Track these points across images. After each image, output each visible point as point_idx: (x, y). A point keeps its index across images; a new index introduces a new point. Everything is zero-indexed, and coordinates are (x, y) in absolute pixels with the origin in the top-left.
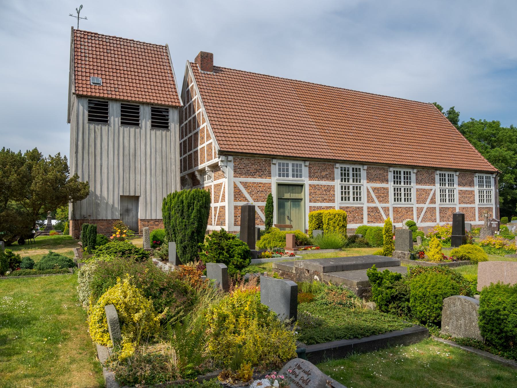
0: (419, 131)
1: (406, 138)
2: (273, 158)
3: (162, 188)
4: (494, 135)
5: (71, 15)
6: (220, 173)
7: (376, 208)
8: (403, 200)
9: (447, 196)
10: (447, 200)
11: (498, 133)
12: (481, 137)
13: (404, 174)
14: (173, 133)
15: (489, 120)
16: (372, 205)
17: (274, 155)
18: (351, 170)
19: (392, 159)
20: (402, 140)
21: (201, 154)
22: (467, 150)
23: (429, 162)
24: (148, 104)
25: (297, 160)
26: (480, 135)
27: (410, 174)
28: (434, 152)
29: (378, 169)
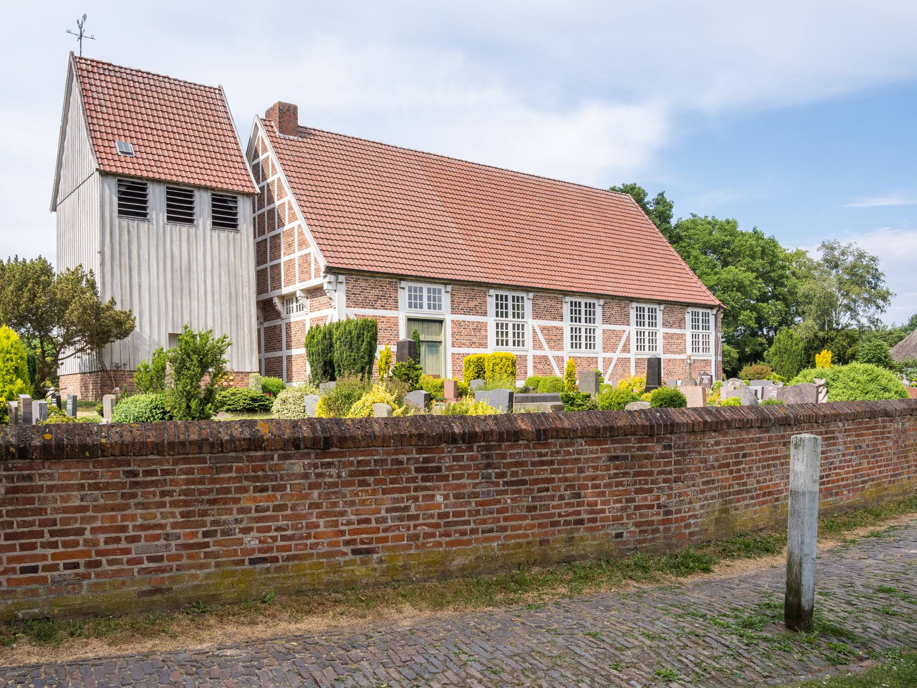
0: (607, 239)
1: (589, 250)
2: (401, 280)
3: (231, 323)
4: (726, 244)
5: (69, 32)
6: (322, 299)
7: (545, 358)
8: (583, 345)
9: (646, 341)
10: (647, 348)
11: (734, 241)
12: (707, 248)
13: (513, 301)
14: (244, 237)
15: (721, 218)
16: (540, 353)
17: (402, 275)
18: (510, 299)
19: (568, 284)
20: (583, 254)
21: (287, 271)
22: (678, 270)
23: (622, 290)
24: (206, 188)
25: (435, 283)
26: (705, 243)
27: (523, 301)
28: (630, 273)
29: (549, 297)
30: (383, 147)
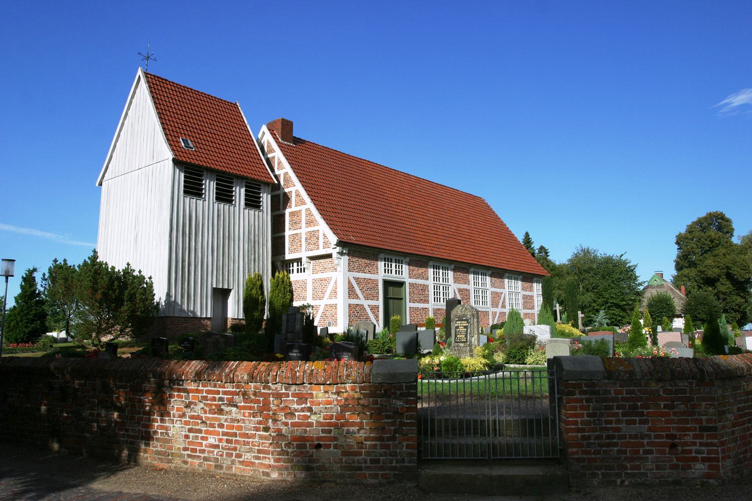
9: (441, 294)
16: (354, 302)
30: (377, 166)
